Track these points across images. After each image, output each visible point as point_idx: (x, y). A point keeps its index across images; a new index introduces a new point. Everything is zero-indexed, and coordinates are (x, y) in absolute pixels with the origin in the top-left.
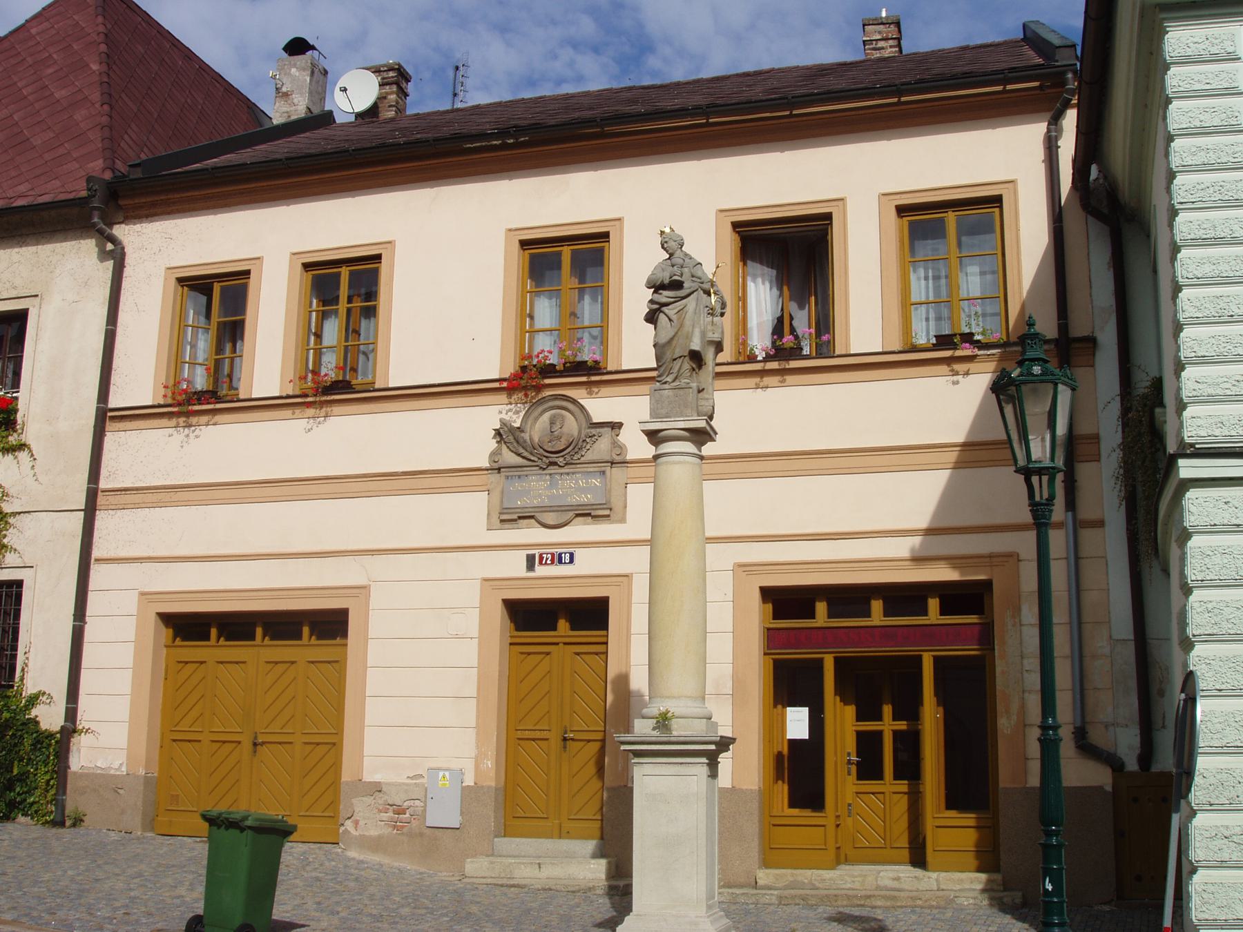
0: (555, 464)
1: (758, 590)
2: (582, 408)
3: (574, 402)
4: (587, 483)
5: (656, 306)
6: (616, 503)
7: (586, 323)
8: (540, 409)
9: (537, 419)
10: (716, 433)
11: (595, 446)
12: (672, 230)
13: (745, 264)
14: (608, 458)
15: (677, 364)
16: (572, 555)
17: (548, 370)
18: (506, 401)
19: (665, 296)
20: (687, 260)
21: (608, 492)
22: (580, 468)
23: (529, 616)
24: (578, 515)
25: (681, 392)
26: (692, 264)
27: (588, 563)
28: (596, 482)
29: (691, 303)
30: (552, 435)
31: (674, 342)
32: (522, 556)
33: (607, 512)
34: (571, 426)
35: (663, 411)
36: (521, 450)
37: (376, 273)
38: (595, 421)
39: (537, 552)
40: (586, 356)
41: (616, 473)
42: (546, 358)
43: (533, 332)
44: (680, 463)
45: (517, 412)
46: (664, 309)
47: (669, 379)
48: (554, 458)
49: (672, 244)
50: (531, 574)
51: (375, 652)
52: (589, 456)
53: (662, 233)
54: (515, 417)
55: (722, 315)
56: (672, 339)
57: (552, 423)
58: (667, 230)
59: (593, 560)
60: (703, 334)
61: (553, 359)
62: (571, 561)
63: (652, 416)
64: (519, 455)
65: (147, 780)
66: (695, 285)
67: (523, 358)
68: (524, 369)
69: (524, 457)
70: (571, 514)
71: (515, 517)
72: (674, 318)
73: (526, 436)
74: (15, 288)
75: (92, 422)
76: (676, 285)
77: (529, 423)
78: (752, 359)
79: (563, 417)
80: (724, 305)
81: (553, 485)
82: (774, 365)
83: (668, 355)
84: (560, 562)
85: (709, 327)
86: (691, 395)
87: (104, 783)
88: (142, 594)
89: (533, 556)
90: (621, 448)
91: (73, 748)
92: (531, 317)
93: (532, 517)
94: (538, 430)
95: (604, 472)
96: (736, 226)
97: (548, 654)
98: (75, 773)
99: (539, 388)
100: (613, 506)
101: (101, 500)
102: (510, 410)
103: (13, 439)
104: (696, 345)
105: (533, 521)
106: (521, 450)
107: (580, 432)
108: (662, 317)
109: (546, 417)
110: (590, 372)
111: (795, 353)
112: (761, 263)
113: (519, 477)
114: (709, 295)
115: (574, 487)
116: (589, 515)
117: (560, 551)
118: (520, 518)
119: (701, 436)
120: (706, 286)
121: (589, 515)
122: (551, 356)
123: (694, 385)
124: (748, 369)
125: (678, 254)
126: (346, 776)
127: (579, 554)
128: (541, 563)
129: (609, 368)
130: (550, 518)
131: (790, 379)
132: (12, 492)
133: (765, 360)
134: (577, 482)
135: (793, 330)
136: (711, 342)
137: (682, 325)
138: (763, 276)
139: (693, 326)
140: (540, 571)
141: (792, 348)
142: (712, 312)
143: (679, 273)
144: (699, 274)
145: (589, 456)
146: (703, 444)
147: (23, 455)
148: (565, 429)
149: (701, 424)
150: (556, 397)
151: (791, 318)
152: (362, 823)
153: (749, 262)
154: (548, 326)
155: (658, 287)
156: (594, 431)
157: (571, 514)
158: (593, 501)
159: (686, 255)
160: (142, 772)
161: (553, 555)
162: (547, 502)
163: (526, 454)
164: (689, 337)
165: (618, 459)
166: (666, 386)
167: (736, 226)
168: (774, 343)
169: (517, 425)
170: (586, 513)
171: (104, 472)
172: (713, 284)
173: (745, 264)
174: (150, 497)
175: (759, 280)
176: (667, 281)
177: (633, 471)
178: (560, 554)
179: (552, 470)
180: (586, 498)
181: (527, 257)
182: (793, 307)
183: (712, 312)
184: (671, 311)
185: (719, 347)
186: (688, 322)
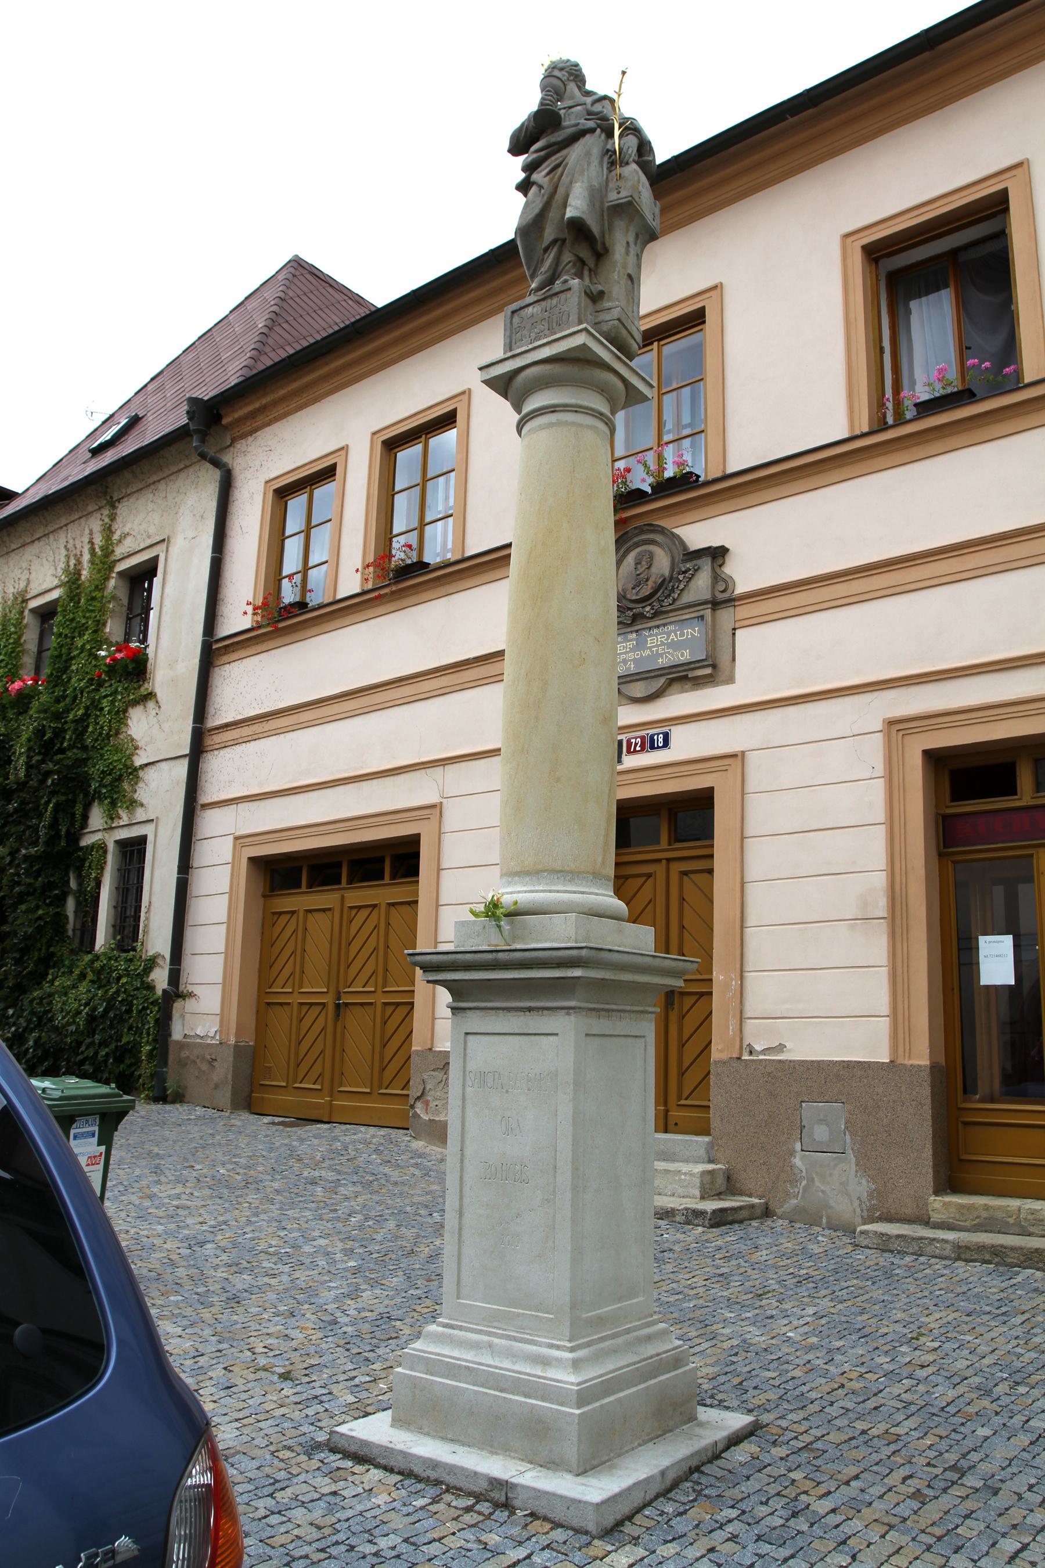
1: (920, 754)
11: (692, 584)
21: (712, 642)
23: (634, 821)
24: (671, 681)
25: (555, 301)
27: (687, 744)
29: (575, 153)
33: (708, 671)
37: (1002, 236)
38: (692, 548)
39: (624, 737)
41: (726, 617)
51: (763, 859)
52: (688, 598)
59: (694, 738)
62: (666, 744)
65: (934, 1067)
70: (662, 680)
74: (149, 537)
75: (196, 661)
79: (651, 556)
87: (208, 1055)
88: (236, 838)
90: (728, 583)
91: (176, 1015)
95: (702, 617)
97: (649, 876)
98: (178, 1042)
101: (212, 740)
103: (143, 691)
104: (577, 206)
107: (672, 570)
116: (686, 677)
117: (651, 732)
121: (686, 677)
126: (718, 1052)
127: (677, 733)
128: (629, 752)
132: (140, 744)
140: (630, 761)
145: (688, 598)
147: (151, 704)
152: (432, 1104)
160: (232, 1041)
161: (643, 738)
162: (632, 668)
164: (565, 205)
165: (721, 597)
171: (211, 710)
174: (246, 731)
177: (743, 611)
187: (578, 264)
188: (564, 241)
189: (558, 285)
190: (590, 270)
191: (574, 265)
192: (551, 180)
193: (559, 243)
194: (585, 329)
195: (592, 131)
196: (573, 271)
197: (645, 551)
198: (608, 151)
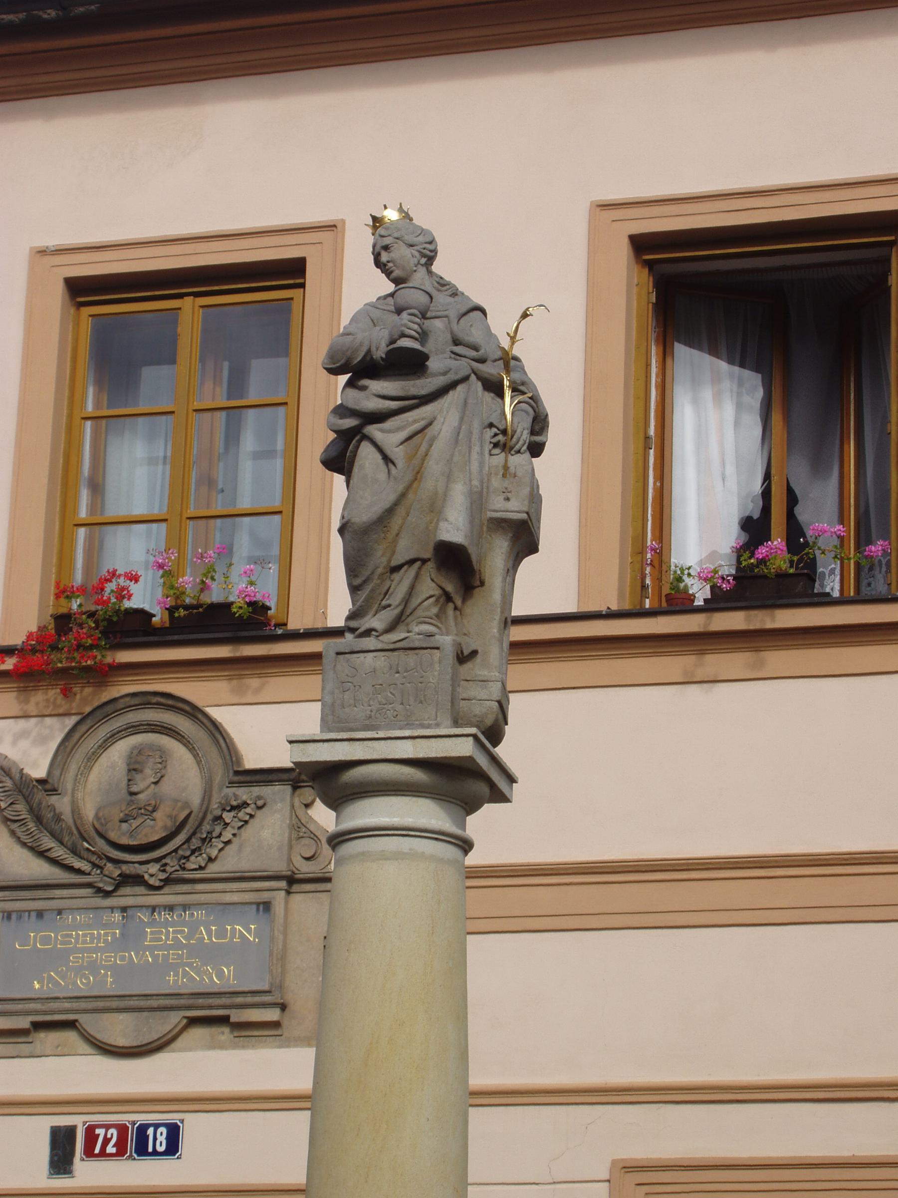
0: (137, 880)
2: (215, 729)
3: (194, 712)
4: (221, 933)
5: (349, 423)
6: (302, 991)
7: (245, 503)
8: (104, 731)
9: (93, 757)
10: (511, 779)
11: (248, 833)
12: (406, 216)
13: (666, 353)
14: (281, 867)
15: (401, 584)
16: (174, 1132)
17: (133, 627)
18: (15, 710)
19: (377, 393)
20: (442, 298)
21: (280, 959)
22: (203, 894)
24: (193, 1022)
25: (411, 659)
26: (454, 308)
28: (245, 931)
29: (446, 414)
30: (136, 808)
31: (396, 522)
32: (36, 1133)
33: (272, 1015)
34: (185, 778)
35: (359, 713)
36: (47, 842)
38: (250, 763)
39: (79, 1122)
40: (233, 588)
42: (122, 594)
43: (99, 525)
44: (398, 856)
45: (42, 740)
46: (373, 430)
47: (377, 622)
48: (133, 864)
49: (402, 254)
50: (61, 1183)
53: (377, 222)
54: (35, 752)
55: (536, 450)
56: (390, 511)
57: (134, 769)
58: (392, 215)
60: (477, 501)
61: (145, 596)
62: (173, 1148)
63: (325, 724)
64: (42, 854)
66: (462, 367)
67: (64, 592)
68: (63, 621)
69: (54, 862)
70: (175, 1019)
71: (24, 1023)
72: (398, 453)
73: (62, 804)
76: (406, 362)
77: (73, 767)
78: (678, 602)
79: (163, 757)
80: (539, 423)
81: (129, 939)
82: (733, 620)
83: (379, 559)
84: (142, 1150)
85: (496, 482)
86: (439, 667)
89: (71, 1131)
92: (97, 487)
93: (71, 1025)
94: (96, 787)
95: (266, 906)
96: (641, 245)
99: (104, 674)
100: (289, 998)
102: (24, 734)
104: (454, 528)
105: (71, 1036)
106: (47, 842)
108: (366, 455)
109: (120, 750)
110: (235, 631)
111: (799, 585)
112: (714, 352)
113: (40, 914)
114: (501, 395)
115: (188, 943)
116: (223, 1020)
117: (142, 1118)
118: (38, 1026)
119: (467, 783)
120: (490, 369)
122: (134, 588)
123: (446, 641)
124: (659, 622)
125: (419, 277)
127: (194, 1128)
128: (89, 1152)
129: (295, 623)
130: (119, 1029)
131: (778, 659)
133: (711, 606)
134: (194, 930)
135: (795, 532)
136: (500, 524)
137: (418, 475)
138: (716, 379)
139: (449, 478)
140: (88, 1173)
141: (781, 576)
142: (503, 442)
143: (413, 328)
144: (475, 335)
146: (470, 806)
148: (166, 787)
149: (462, 748)
150: (146, 700)
151: (792, 499)
153: (681, 350)
154: (140, 509)
155: (360, 368)
156: (244, 794)
157: (175, 1019)
158: (234, 984)
159: (442, 284)
161: (122, 1129)
162: (110, 985)
163: (58, 852)
164: (436, 508)
165: (306, 869)
166: (370, 643)
167: (641, 245)
168: (740, 551)
169: (40, 772)
170: (217, 1016)
172: (508, 361)
173: (666, 353)
175: (707, 394)
176: (380, 353)
178: (142, 1130)
179: (130, 896)
180: (221, 976)
181: (86, 325)
182: (799, 474)
183: (503, 442)
184: (388, 435)
185: (524, 538)
186: (434, 468)
187: (442, 600)
188: (424, 561)
189: (417, 630)
190: (456, 608)
191: (437, 601)
192: (410, 457)
193: (418, 564)
194: (475, 736)
195: (466, 379)
196: (435, 610)
197: (153, 747)
198: (491, 425)
